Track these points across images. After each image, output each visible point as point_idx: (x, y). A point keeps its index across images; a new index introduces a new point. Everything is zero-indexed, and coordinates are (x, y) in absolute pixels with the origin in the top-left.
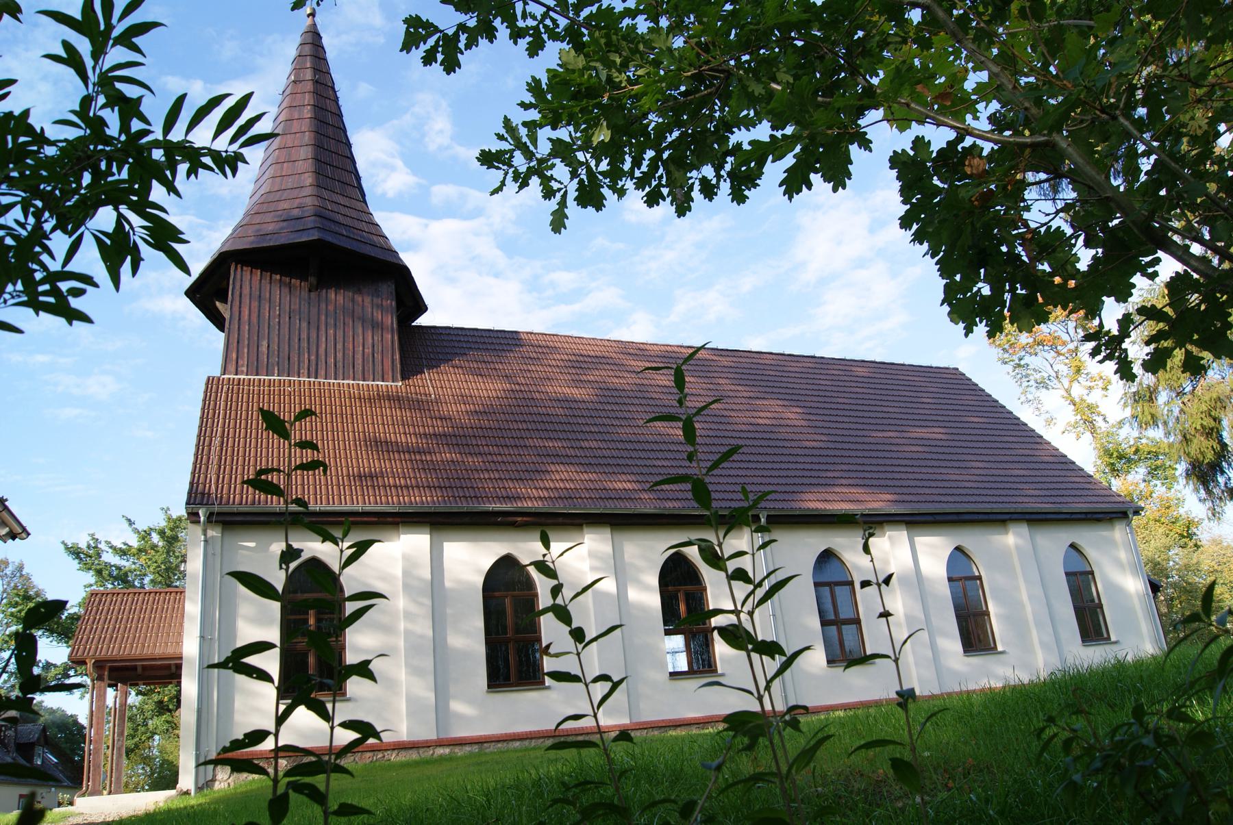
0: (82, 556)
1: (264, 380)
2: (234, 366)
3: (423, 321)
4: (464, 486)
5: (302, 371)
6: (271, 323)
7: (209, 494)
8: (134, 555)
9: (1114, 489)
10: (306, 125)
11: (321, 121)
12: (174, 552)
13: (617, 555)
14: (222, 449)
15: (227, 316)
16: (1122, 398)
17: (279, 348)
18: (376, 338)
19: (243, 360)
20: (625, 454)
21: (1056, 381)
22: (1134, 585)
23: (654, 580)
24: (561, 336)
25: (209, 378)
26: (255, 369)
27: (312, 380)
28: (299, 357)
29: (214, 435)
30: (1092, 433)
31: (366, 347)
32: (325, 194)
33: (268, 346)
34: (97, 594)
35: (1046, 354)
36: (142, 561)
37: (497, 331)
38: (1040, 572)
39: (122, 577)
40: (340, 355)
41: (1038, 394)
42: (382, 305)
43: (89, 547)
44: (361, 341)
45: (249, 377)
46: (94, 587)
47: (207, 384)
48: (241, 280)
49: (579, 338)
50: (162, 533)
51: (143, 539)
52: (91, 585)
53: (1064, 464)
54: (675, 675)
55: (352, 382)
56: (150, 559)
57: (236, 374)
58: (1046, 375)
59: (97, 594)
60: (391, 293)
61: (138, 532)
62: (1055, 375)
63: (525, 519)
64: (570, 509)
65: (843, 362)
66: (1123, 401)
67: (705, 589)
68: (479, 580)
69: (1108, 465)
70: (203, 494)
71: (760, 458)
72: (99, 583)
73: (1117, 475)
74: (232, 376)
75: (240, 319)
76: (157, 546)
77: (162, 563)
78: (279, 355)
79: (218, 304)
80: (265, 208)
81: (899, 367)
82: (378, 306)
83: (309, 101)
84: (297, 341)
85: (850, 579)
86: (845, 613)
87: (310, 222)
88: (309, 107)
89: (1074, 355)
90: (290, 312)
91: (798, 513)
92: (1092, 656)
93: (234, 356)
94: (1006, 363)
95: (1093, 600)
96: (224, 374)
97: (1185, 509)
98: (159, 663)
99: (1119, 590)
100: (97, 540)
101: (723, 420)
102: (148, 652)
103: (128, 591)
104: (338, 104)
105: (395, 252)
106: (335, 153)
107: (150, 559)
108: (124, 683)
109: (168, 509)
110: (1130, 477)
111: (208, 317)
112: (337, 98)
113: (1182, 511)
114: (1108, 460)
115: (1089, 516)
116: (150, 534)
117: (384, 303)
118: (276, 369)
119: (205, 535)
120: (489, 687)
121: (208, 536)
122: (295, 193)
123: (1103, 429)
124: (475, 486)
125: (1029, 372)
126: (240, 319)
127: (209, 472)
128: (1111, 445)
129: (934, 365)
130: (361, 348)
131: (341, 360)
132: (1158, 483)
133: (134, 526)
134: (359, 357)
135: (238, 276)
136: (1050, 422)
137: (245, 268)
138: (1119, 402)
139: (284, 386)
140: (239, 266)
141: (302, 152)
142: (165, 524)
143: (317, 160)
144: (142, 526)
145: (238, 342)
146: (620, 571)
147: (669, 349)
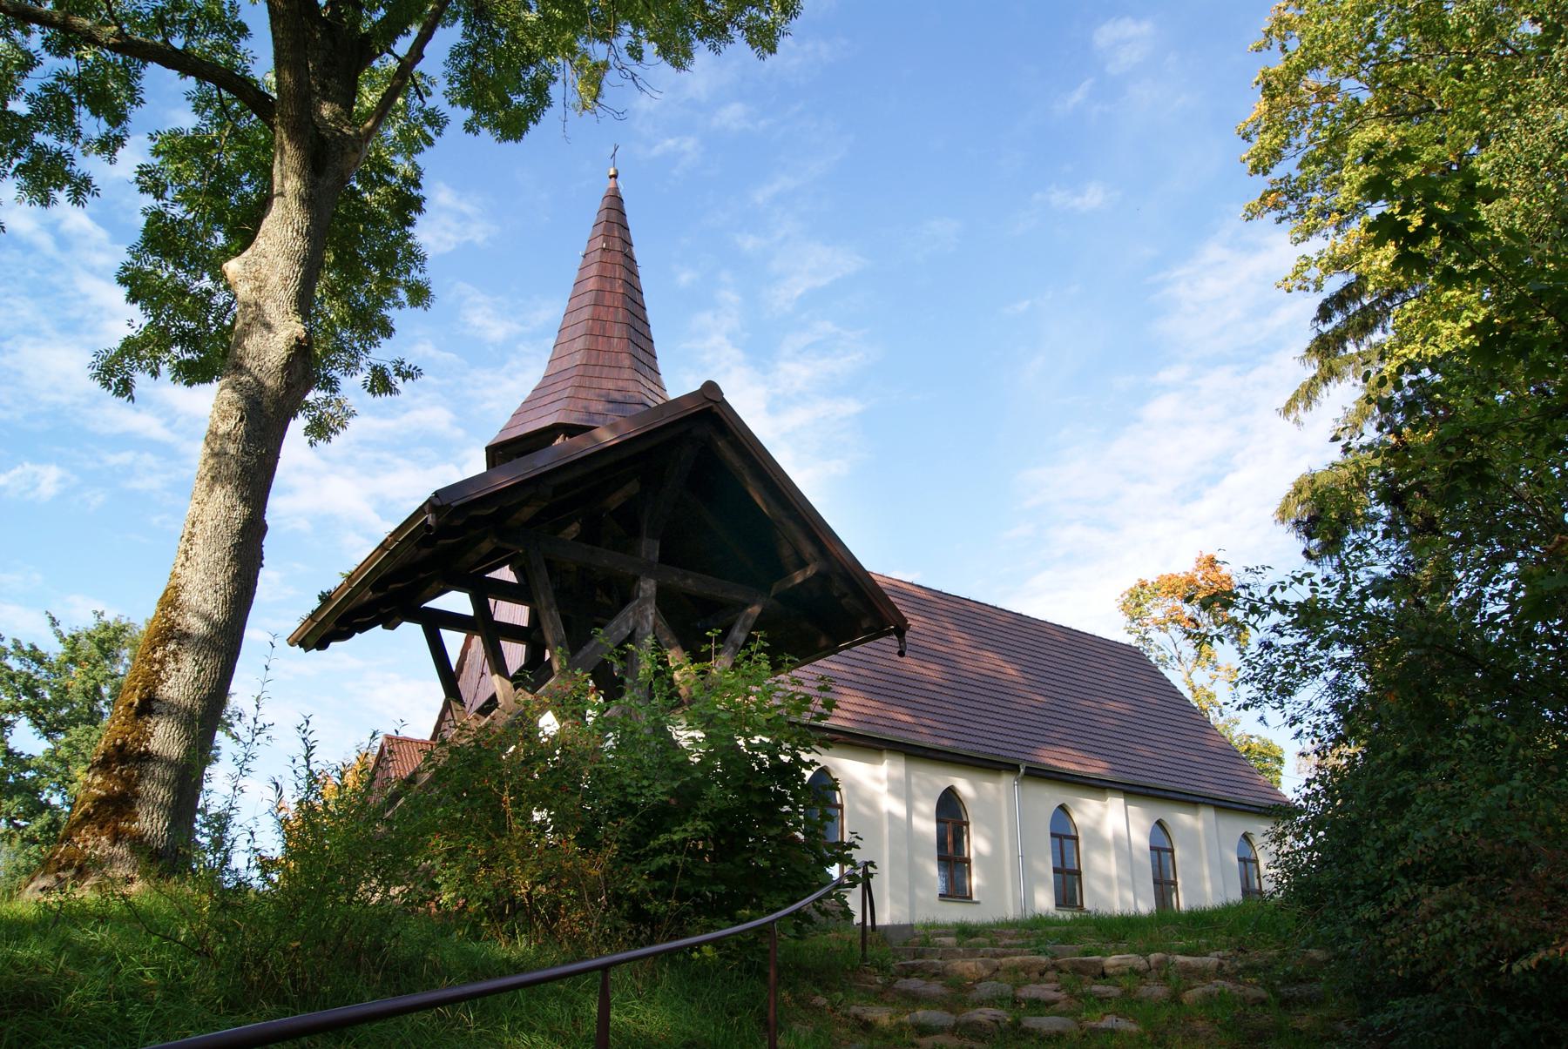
58: (1169, 655)
92: (954, 913)
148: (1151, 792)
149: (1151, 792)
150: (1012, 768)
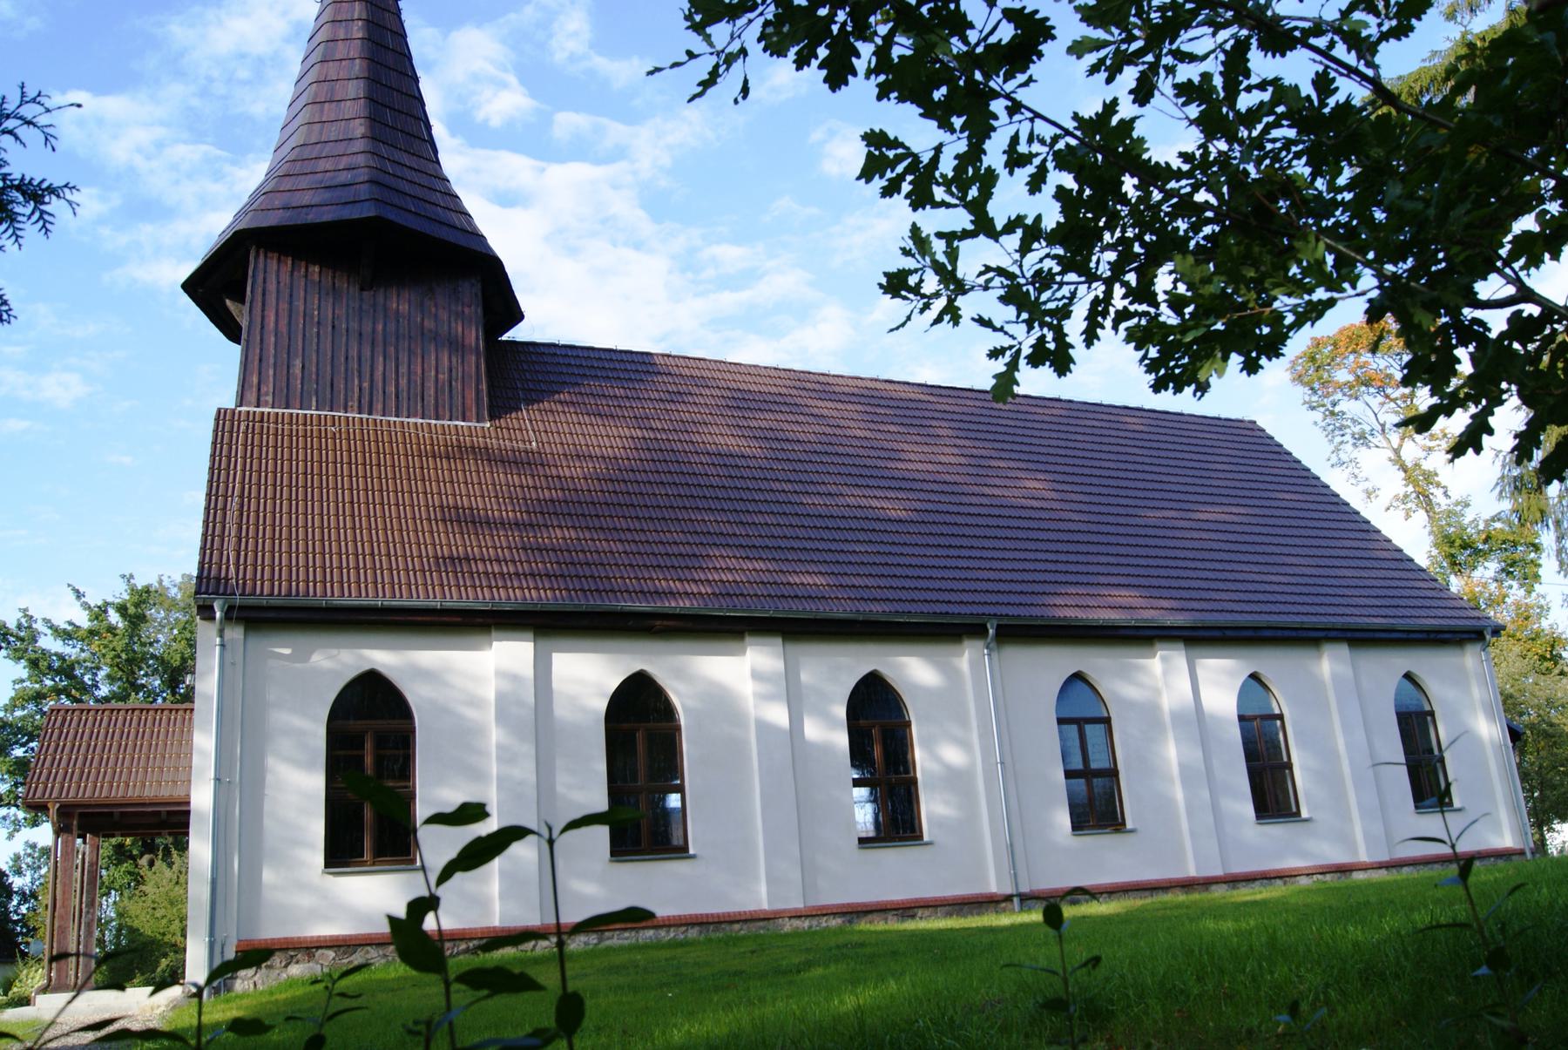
0: (12, 639)
1: (298, 415)
2: (255, 395)
3: (518, 333)
4: (582, 574)
5: (350, 404)
6: (307, 335)
7: (227, 579)
8: (83, 640)
9: (1454, 589)
10: (355, 49)
11: (377, 44)
12: (140, 637)
13: (791, 675)
14: (242, 514)
15: (244, 324)
16: (1497, 484)
17: (318, 370)
18: (454, 360)
19: (267, 386)
20: (801, 533)
21: (1380, 437)
22: (1488, 730)
23: (841, 712)
24: (710, 361)
25: (219, 410)
26: (284, 400)
27: (365, 416)
28: (346, 384)
29: (230, 493)
30: (1427, 511)
31: (440, 370)
32: (384, 150)
33: (303, 367)
34: (59, 711)
35: (1367, 398)
36: (94, 648)
37: (621, 352)
38: (1362, 710)
39: (66, 669)
40: (403, 382)
41: (1355, 454)
42: (463, 312)
43: (19, 626)
44: (433, 362)
45: (276, 410)
46: (27, 684)
47: (217, 419)
48: (265, 272)
49: (735, 364)
50: (122, 609)
51: (97, 618)
52: (22, 681)
53: (1401, 560)
54: (863, 841)
55: (421, 421)
56: (106, 647)
57: (258, 406)
59: (59, 711)
60: (476, 295)
61: (90, 607)
62: (1379, 428)
63: (665, 623)
64: (730, 611)
65: (1098, 409)
66: (1498, 489)
67: (909, 724)
68: (603, 705)
69: (1446, 557)
70: (218, 579)
71: (986, 543)
72: (34, 678)
73: (1460, 571)
74: (252, 409)
75: (262, 328)
76: (115, 628)
77: (122, 651)
78: (317, 380)
79: (228, 302)
80: (298, 168)
81: (1175, 418)
82: (457, 314)
83: (360, 14)
84: (343, 359)
85: (1106, 715)
86: (1098, 762)
87: (364, 191)
88: (360, 23)
89: (1409, 403)
90: (333, 318)
91: (1039, 622)
93: (255, 380)
94: (1313, 408)
95: (1431, 751)
96: (241, 405)
97: (1549, 622)
98: (150, 809)
99: (1464, 734)
100: (32, 617)
101: (893, 454)
102: (134, 793)
103: (103, 707)
104: (400, 19)
105: (483, 236)
106: (398, 91)
107: (106, 647)
108: (95, 833)
109: (132, 576)
110: (1477, 574)
111: (212, 320)
112: (399, 10)
113: (1545, 624)
114: (1447, 549)
115: (1432, 636)
116: (105, 612)
117: (467, 310)
118: (314, 399)
119: (221, 636)
120: (612, 854)
121: (226, 639)
122: (340, 148)
123: (1444, 507)
124: (597, 575)
125: (1345, 423)
126: (262, 328)
127: (225, 547)
128: (1452, 529)
129: (1223, 416)
130: (433, 373)
131: (405, 389)
132: (1515, 584)
133: (83, 599)
134: (430, 385)
135: (261, 265)
136: (1369, 494)
137: (270, 255)
138: (1494, 488)
139: (326, 425)
140: (262, 251)
141: (350, 86)
142: (127, 597)
143: (371, 99)
144: (95, 600)
145: (260, 360)
146: (795, 699)
147: (860, 383)
148: (1229, 633)
149: (1229, 633)
150: (974, 630)
